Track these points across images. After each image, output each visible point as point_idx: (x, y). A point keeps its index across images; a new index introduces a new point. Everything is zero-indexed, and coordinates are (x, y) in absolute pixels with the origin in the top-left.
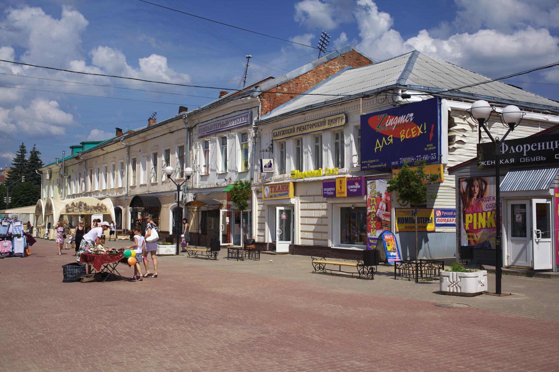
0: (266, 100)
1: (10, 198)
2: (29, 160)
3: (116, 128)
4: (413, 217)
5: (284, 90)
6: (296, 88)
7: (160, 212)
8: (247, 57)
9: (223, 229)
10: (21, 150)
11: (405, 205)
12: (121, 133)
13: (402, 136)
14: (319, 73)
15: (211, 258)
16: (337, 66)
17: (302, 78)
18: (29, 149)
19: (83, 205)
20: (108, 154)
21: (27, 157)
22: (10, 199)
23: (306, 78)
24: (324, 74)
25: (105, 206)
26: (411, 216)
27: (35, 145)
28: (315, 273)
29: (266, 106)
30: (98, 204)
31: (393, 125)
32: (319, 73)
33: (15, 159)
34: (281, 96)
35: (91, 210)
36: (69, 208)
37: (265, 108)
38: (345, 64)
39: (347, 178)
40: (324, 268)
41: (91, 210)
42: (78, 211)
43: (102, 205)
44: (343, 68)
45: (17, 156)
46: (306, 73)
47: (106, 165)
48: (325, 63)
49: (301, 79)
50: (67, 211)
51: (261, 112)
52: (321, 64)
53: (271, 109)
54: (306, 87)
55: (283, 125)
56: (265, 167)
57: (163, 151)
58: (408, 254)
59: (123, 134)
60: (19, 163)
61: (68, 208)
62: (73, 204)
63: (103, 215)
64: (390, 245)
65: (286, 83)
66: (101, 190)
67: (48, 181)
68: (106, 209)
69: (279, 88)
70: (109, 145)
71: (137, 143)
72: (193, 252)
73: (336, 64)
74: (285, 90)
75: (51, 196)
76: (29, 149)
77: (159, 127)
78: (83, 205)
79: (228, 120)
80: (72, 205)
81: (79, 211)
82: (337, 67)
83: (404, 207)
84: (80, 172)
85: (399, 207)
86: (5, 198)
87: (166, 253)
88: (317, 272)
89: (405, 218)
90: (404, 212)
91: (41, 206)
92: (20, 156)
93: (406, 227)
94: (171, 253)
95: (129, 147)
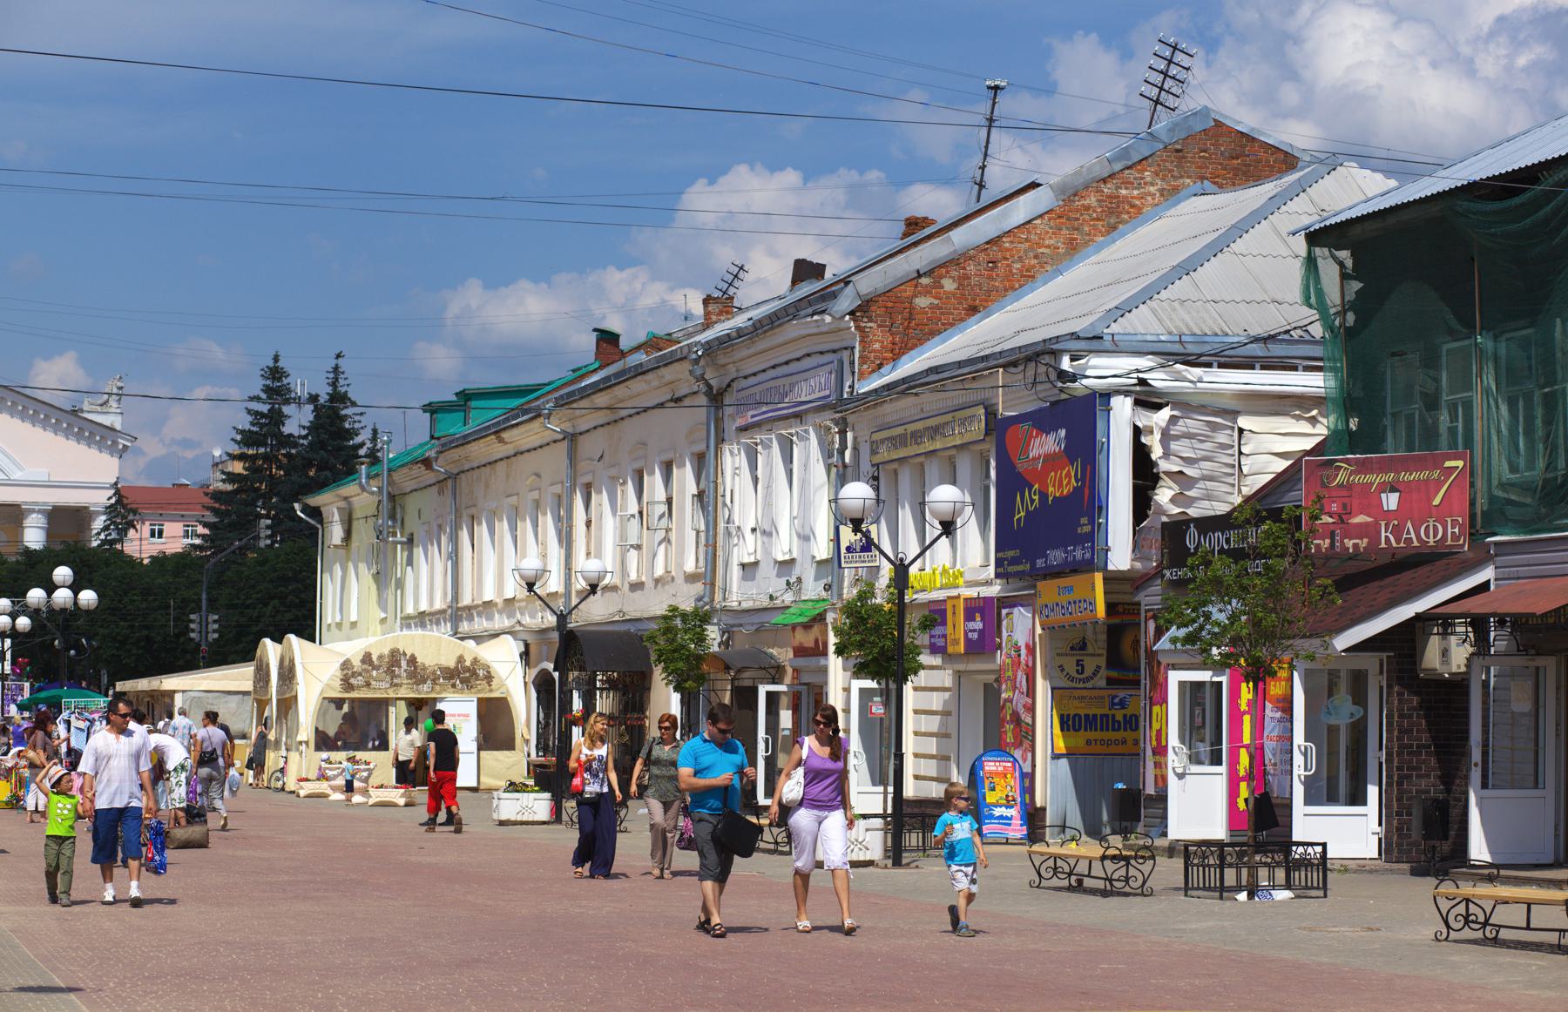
0: (879, 326)
1: (216, 617)
2: (305, 437)
3: (595, 330)
4: (1113, 712)
5: (942, 287)
6: (990, 278)
7: (649, 689)
8: (989, 87)
9: (767, 751)
10: (267, 389)
11: (1084, 681)
12: (617, 351)
13: (1051, 489)
14: (1077, 219)
15: (1127, 889)
16: (1152, 184)
17: (1012, 242)
18: (307, 381)
19: (404, 664)
20: (519, 457)
21: (297, 421)
22: (215, 622)
23: (1027, 240)
24: (1098, 219)
25: (487, 668)
26: (1106, 711)
27: (338, 356)
28: (1446, 939)
29: (877, 346)
30: (461, 659)
31: (1040, 456)
32: (1077, 219)
33: (241, 432)
34: (932, 307)
35: (434, 681)
36: (354, 675)
37: (875, 351)
38: (1182, 177)
39: (966, 599)
40: (1487, 920)
41: (434, 681)
42: (385, 685)
43: (475, 661)
44: (1175, 190)
45: (250, 418)
46: (1029, 222)
47: (513, 500)
48: (1104, 181)
49: (1007, 245)
50: (347, 685)
51: (861, 364)
52: (1087, 187)
53: (897, 352)
54: (1027, 271)
55: (890, 419)
56: (849, 549)
57: (630, 471)
58: (1105, 817)
59: (623, 355)
60: (262, 450)
61: (348, 675)
62: (367, 658)
63: (479, 699)
64: (998, 788)
65: (950, 261)
66: (499, 601)
67: (342, 552)
68: (489, 678)
69: (925, 281)
70: (517, 425)
71: (595, 428)
72: (1059, 863)
73: (1149, 179)
74: (949, 285)
75: (349, 617)
76: (307, 381)
77: (639, 378)
78: (404, 664)
79: (795, 378)
80: (363, 661)
81: (388, 686)
82: (1152, 189)
83: (1081, 685)
84: (440, 521)
85: (1067, 686)
86: (192, 617)
87: (519, 818)
88: (1453, 935)
89: (1087, 716)
90: (1083, 698)
91: (268, 665)
92: (262, 415)
93: (1089, 742)
94: (537, 818)
95: (572, 438)
